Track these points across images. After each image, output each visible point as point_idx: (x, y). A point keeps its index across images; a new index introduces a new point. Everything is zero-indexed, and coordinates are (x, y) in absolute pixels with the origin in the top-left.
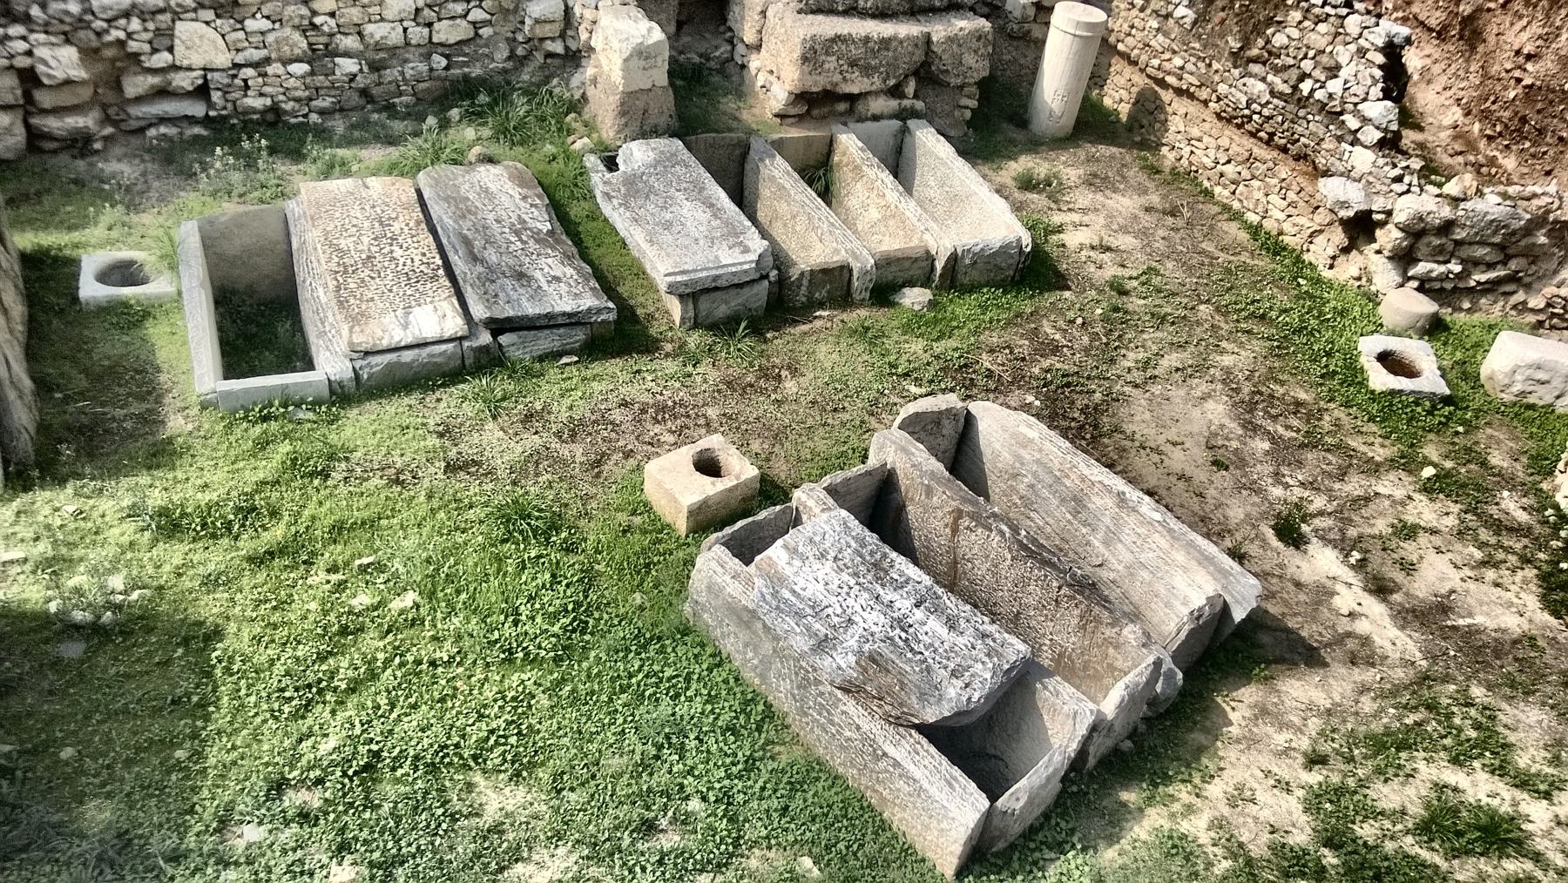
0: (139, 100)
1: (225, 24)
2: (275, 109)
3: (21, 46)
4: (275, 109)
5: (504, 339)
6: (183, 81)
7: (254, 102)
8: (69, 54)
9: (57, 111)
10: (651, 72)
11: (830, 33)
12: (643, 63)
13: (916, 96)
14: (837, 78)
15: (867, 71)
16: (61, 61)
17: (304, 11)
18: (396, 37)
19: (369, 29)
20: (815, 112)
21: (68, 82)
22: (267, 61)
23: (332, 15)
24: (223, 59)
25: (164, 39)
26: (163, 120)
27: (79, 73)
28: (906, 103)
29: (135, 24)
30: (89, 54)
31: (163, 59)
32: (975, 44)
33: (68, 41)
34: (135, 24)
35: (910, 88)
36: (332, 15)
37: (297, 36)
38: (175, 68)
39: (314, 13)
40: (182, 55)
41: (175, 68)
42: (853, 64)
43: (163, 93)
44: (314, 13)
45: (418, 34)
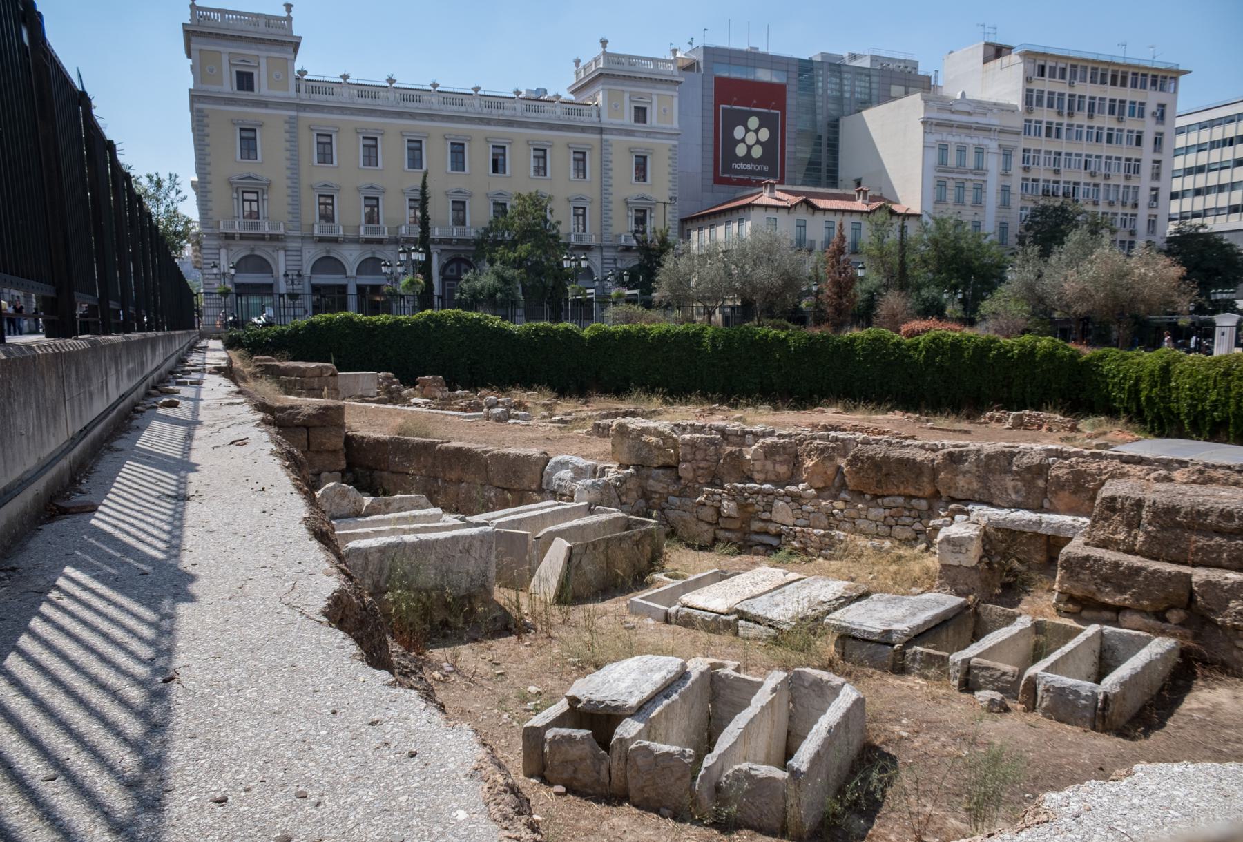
0: (757, 533)
1: (794, 505)
3: (718, 497)
5: (742, 622)
9: (726, 529)
11: (1085, 554)
12: (951, 548)
16: (728, 507)
19: (858, 522)
21: (729, 517)
23: (842, 510)
25: (769, 507)
27: (734, 514)
29: (759, 498)
30: (742, 507)
31: (766, 515)
33: (734, 500)
34: (759, 498)
36: (842, 510)
37: (823, 518)
38: (770, 521)
40: (777, 517)
41: (770, 521)
43: (767, 533)
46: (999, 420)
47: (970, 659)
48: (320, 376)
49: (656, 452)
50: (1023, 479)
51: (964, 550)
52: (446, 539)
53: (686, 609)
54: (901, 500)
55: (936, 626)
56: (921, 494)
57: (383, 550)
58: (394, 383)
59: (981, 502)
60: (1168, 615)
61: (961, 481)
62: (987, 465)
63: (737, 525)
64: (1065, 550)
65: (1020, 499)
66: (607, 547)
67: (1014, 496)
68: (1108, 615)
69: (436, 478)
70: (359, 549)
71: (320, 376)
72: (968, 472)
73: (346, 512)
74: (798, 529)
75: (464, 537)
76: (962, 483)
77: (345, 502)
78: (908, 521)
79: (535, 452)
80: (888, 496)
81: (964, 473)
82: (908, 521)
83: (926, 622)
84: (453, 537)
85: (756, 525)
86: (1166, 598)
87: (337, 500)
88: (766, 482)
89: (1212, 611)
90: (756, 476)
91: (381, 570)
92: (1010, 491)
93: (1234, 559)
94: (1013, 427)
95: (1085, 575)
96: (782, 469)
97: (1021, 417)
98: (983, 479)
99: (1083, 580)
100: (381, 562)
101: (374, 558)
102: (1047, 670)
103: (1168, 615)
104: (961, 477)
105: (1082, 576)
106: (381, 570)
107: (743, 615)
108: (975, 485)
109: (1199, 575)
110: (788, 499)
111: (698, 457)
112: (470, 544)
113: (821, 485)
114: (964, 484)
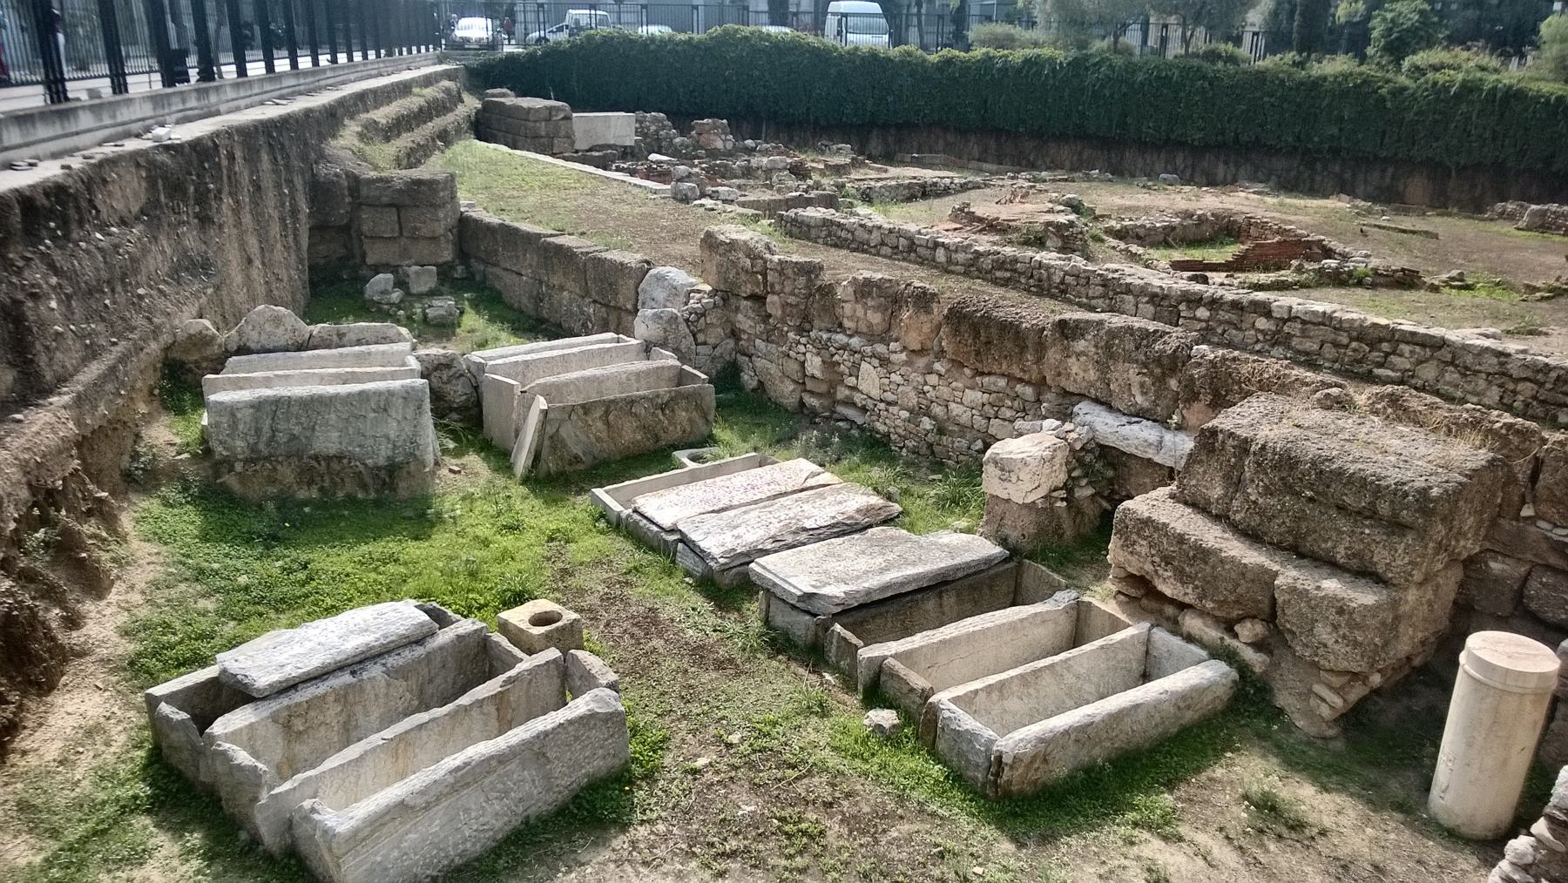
1: (883, 371)
2: (888, 435)
3: (802, 349)
4: (888, 435)
6: (858, 398)
7: (882, 428)
8: (818, 360)
10: (1006, 484)
13: (1258, 645)
14: (1149, 567)
15: (1182, 577)
16: (814, 365)
17: (920, 379)
18: (965, 418)
19: (952, 406)
20: (1144, 602)
22: (896, 404)
24: (875, 393)
26: (846, 419)
27: (818, 374)
28: (1235, 643)
30: (830, 365)
31: (851, 381)
32: (1333, 617)
35: (1248, 630)
37: (912, 394)
39: (926, 383)
42: (1167, 560)
44: (926, 383)
45: (979, 422)
46: (1511, 217)
47: (885, 658)
48: (548, 120)
49: (743, 277)
50: (1151, 374)
51: (1014, 479)
52: (349, 395)
53: (636, 516)
54: (1002, 382)
55: (920, 590)
56: (1026, 377)
57: (258, 406)
58: (664, 127)
59: (1097, 401)
60: (1237, 628)
61: (1074, 366)
62: (1108, 347)
63: (823, 388)
64: (1127, 504)
65: (1146, 405)
66: (607, 413)
67: (1139, 399)
68: (1170, 610)
69: (541, 282)
70: (221, 403)
71: (548, 120)
72: (1082, 353)
73: (282, 342)
74: (882, 406)
75: (378, 393)
76: (1075, 369)
77: (280, 331)
78: (1009, 414)
79: (631, 258)
80: (989, 374)
81: (1078, 355)
82: (1009, 414)
83: (868, 592)
84: (361, 393)
85: (842, 393)
86: (1237, 602)
87: (268, 327)
88: (857, 333)
89: (1293, 633)
90: (847, 323)
91: (258, 431)
92: (1135, 390)
93: (1354, 555)
94: (1528, 229)
95: (1142, 547)
96: (875, 318)
97: (1543, 214)
98: (1103, 368)
99: (1139, 554)
100: (256, 420)
101: (245, 416)
102: (955, 700)
103: (1237, 628)
104: (1073, 359)
105: (1138, 548)
106: (258, 431)
107: (684, 539)
108: (1092, 375)
109: (1289, 575)
110: (876, 362)
111: (787, 290)
112: (387, 402)
113: (917, 347)
114: (1080, 372)
